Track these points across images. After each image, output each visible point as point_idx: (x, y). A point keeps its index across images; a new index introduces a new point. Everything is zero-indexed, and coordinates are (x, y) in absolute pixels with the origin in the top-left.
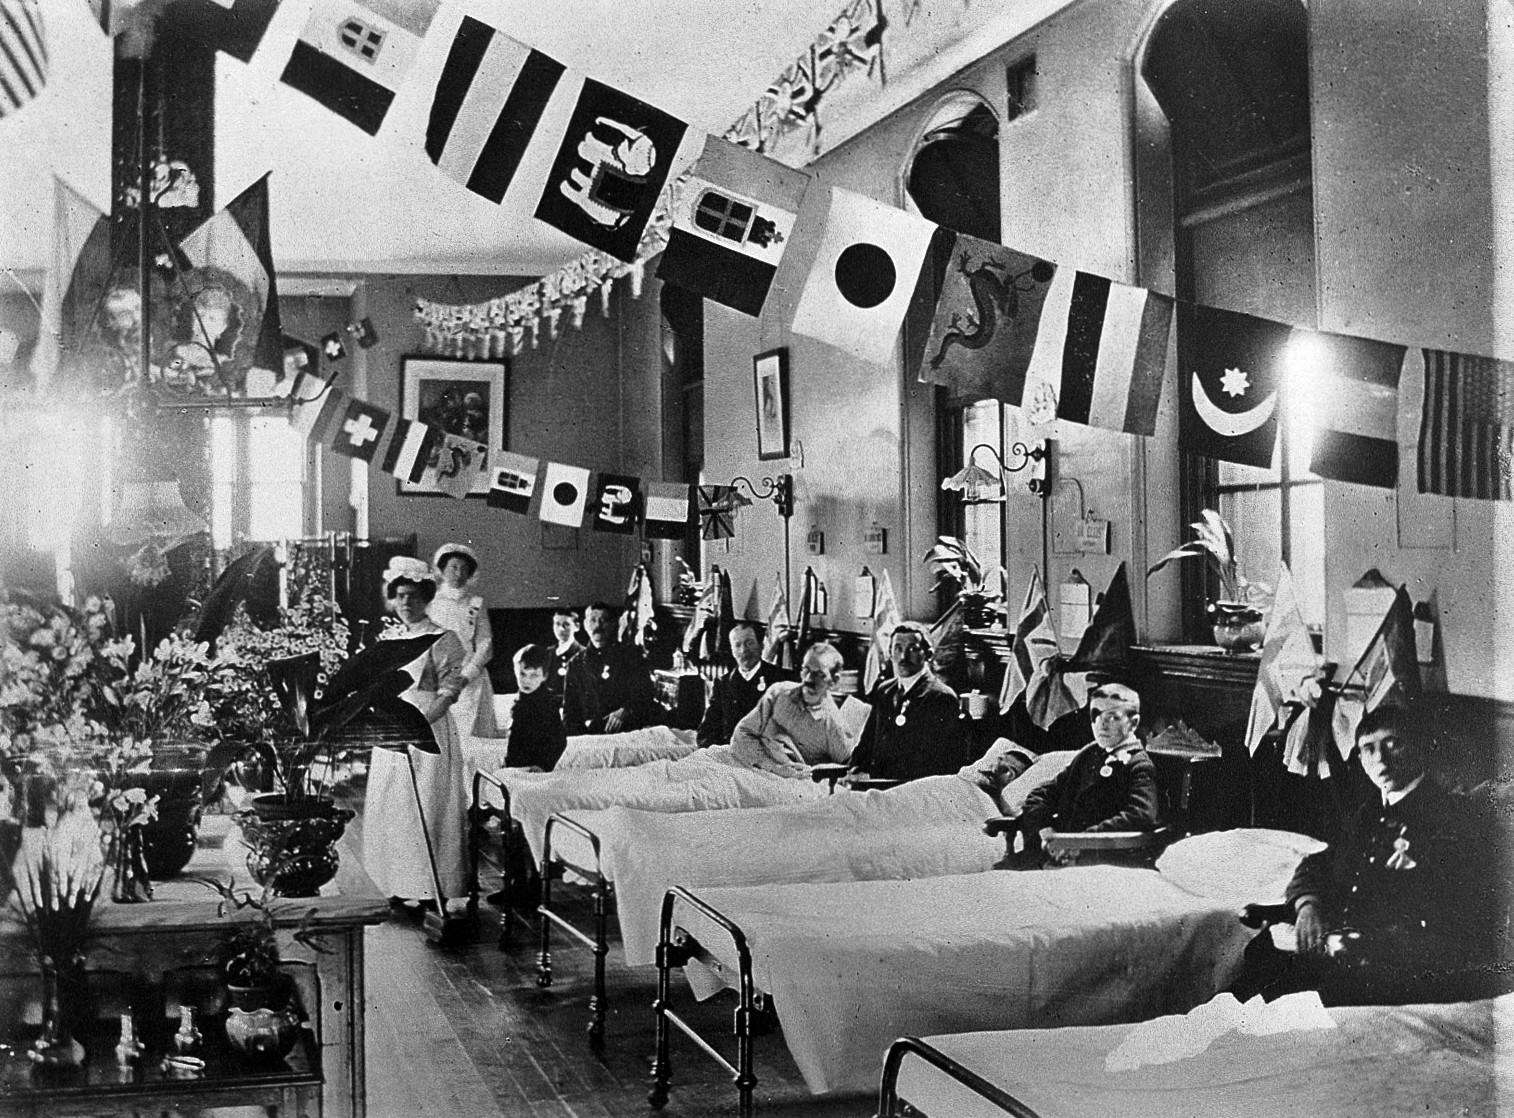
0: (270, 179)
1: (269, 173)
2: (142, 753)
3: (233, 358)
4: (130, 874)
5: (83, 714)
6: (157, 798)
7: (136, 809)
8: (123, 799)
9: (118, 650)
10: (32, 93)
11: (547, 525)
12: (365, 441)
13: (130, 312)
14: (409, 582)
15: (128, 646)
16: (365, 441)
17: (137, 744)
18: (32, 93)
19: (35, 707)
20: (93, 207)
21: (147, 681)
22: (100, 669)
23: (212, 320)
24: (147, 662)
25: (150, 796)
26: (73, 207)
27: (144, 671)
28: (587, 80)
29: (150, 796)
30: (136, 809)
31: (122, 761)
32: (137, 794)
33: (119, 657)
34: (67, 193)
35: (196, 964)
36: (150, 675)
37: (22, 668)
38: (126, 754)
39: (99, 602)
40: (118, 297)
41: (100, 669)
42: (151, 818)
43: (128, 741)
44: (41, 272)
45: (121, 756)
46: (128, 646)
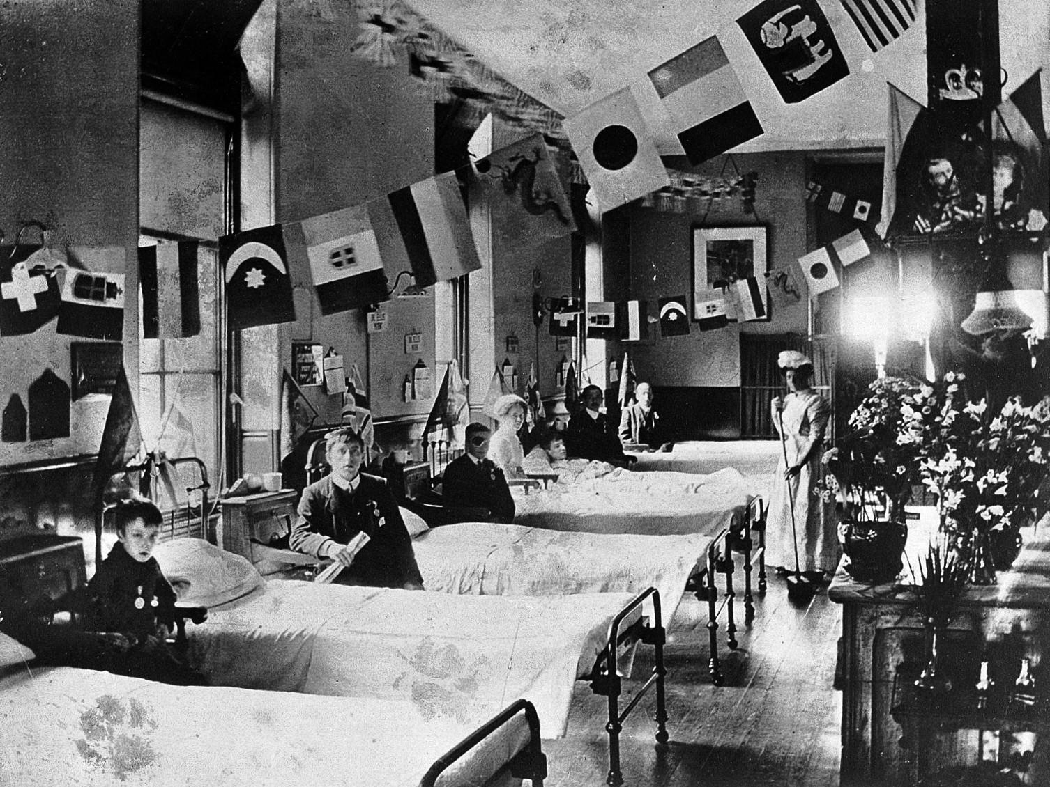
0: (1041, 74)
1: (1040, 70)
2: (1000, 480)
3: (1017, 202)
4: (982, 564)
5: (954, 452)
6: (1011, 512)
7: (996, 519)
8: (987, 512)
9: (976, 409)
10: (905, 26)
11: (641, 338)
12: (15, 301)
13: (943, 173)
14: (791, 369)
15: (982, 407)
16: (15, 301)
17: (997, 475)
18: (905, 26)
19: (919, 447)
20: (919, 104)
21: (998, 431)
22: (963, 421)
23: (1003, 178)
24: (998, 418)
25: (1006, 512)
26: (902, 103)
27: (996, 425)
28: (737, 21)
29: (1006, 512)
30: (996, 519)
31: (986, 486)
32: (997, 510)
33: (975, 413)
34: (897, 92)
35: (907, 631)
36: (1000, 427)
37: (914, 420)
38: (990, 481)
39: (954, 375)
40: (935, 164)
41: (963, 421)
42: (1005, 525)
43: (991, 472)
44: (882, 149)
45: (986, 481)
46: (982, 407)
